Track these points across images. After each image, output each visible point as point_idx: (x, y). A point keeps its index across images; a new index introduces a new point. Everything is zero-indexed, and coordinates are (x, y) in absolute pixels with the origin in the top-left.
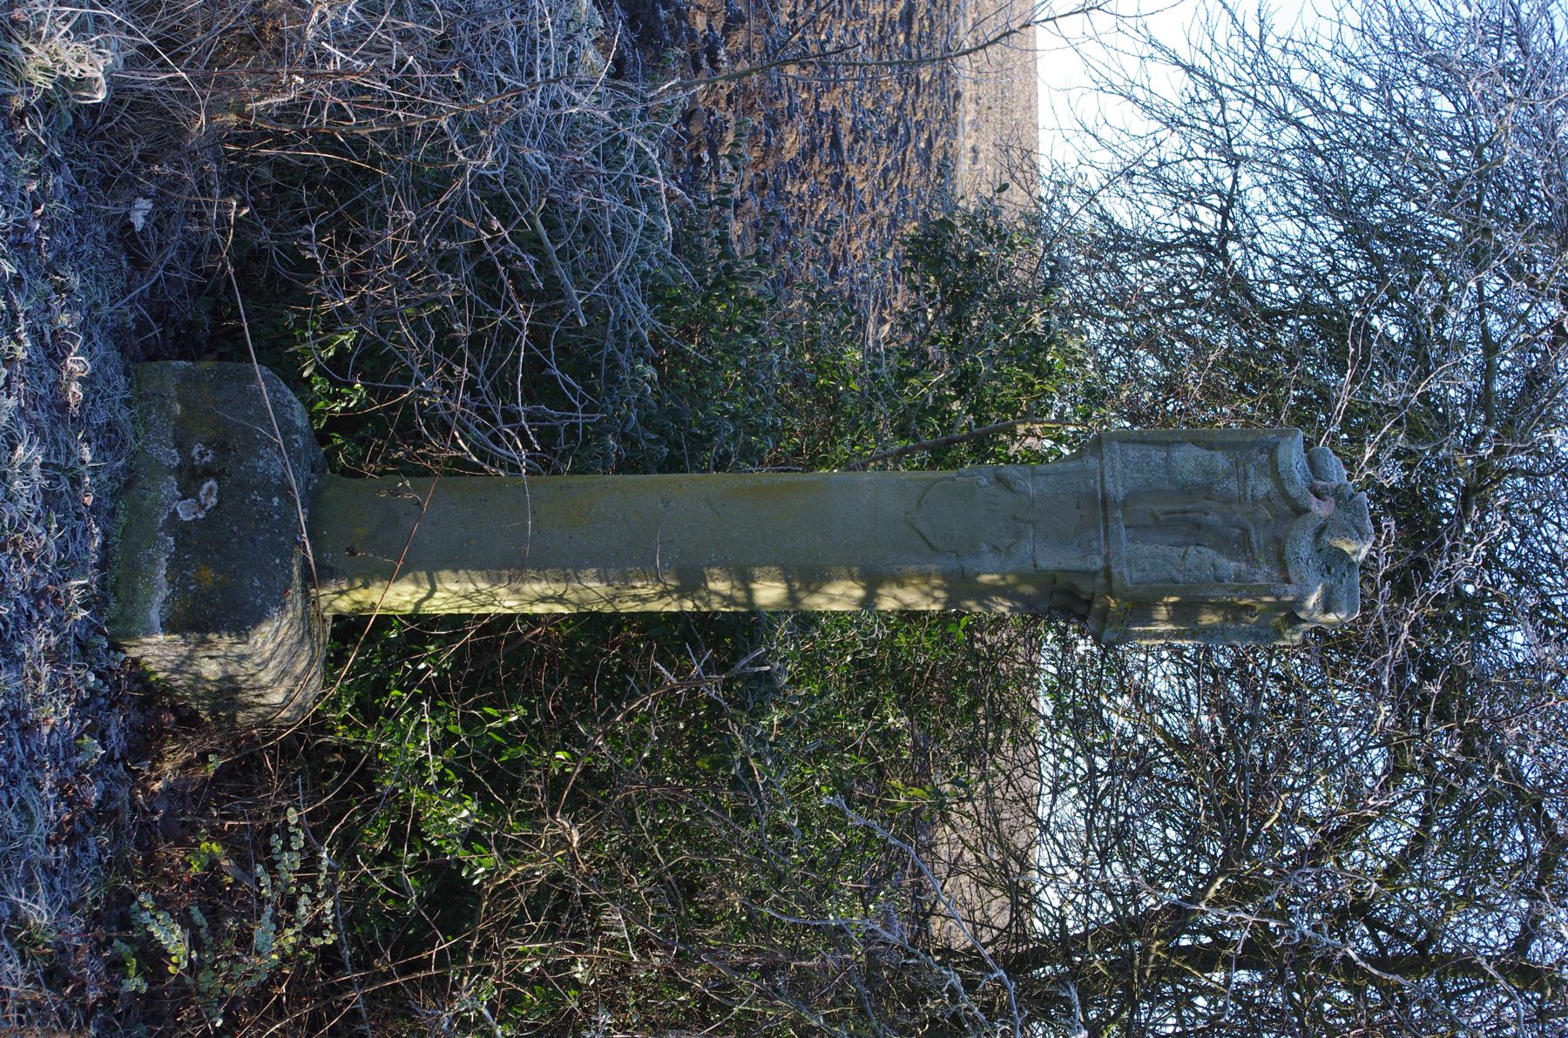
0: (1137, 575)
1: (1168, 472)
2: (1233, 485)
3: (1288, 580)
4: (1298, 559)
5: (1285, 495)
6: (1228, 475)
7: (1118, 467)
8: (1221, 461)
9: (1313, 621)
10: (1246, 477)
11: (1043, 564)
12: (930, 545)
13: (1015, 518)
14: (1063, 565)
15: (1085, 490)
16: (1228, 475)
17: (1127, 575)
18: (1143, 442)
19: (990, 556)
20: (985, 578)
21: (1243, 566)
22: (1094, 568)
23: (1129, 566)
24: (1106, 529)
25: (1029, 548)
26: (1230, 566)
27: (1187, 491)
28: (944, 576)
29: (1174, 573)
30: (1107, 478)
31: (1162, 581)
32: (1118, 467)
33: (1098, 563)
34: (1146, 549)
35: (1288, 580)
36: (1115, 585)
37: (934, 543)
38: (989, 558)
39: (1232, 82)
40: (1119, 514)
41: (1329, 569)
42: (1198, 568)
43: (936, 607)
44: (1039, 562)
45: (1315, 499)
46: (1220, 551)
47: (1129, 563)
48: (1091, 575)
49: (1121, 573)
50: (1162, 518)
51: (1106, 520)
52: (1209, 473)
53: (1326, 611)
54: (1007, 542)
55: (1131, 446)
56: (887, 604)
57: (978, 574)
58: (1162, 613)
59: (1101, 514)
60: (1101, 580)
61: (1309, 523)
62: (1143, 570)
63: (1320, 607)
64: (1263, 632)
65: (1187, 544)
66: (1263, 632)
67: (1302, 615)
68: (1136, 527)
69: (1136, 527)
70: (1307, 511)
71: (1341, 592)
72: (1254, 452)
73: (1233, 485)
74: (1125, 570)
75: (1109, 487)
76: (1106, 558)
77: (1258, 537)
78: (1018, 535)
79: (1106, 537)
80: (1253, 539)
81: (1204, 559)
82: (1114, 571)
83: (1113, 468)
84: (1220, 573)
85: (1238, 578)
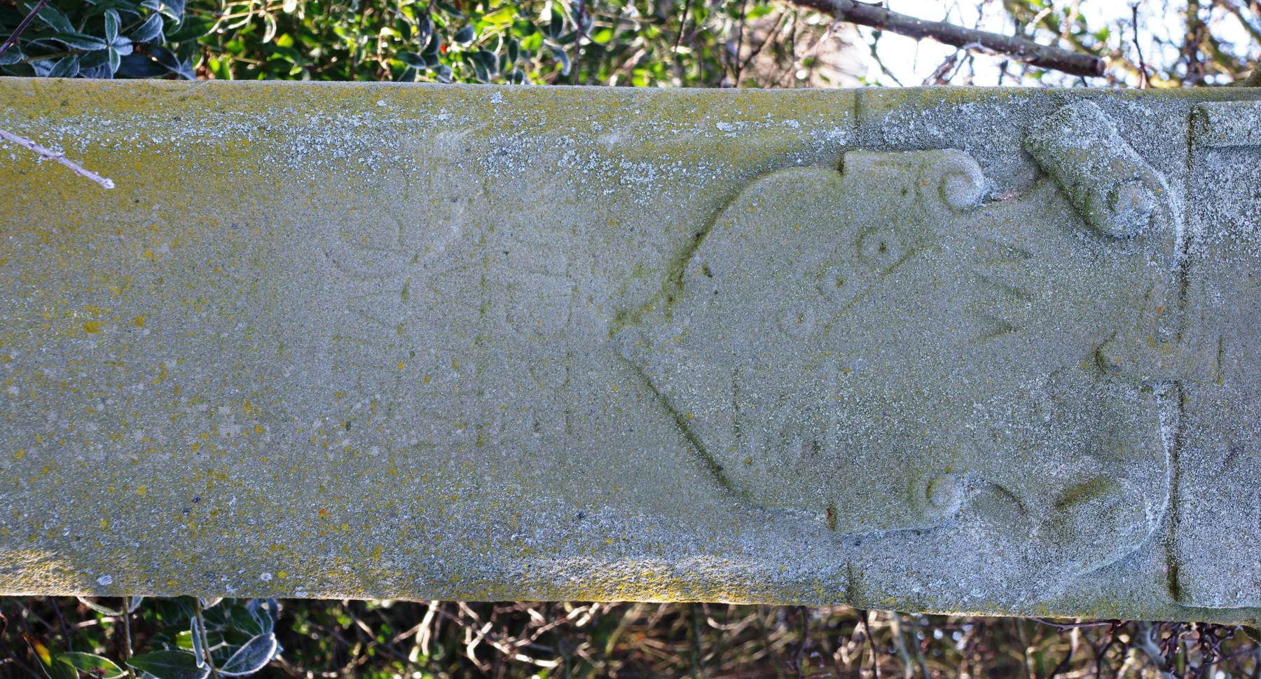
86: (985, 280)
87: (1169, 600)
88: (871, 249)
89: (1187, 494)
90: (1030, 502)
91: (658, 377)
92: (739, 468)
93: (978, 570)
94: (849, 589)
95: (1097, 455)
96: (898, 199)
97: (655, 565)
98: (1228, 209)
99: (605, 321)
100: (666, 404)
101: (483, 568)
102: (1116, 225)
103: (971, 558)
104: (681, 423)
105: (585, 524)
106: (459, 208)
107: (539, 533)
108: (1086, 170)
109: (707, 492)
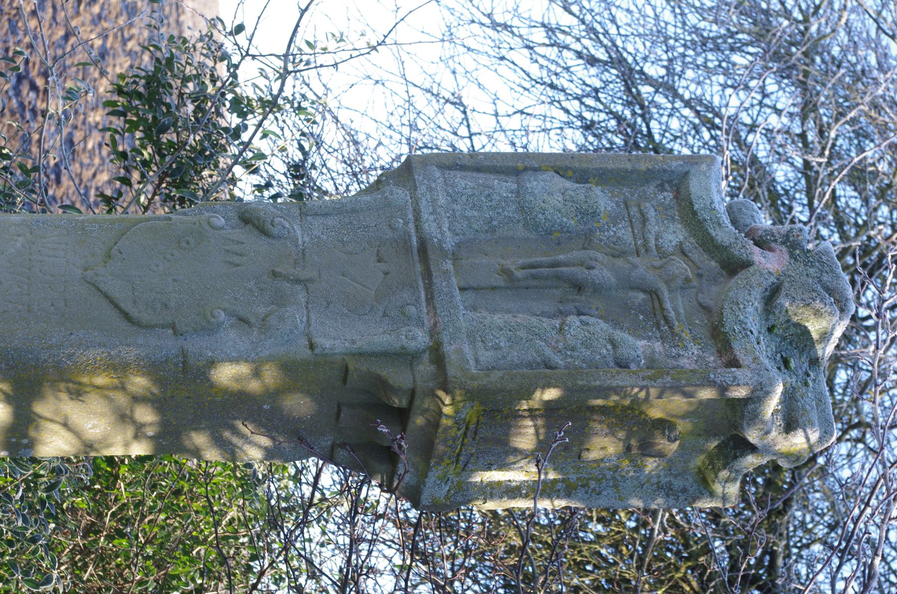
0: (486, 356)
1: (522, 209)
2: (624, 233)
3: (734, 363)
4: (746, 332)
5: (710, 246)
6: (614, 220)
7: (442, 201)
8: (603, 199)
9: (767, 450)
10: (644, 220)
11: (325, 343)
12: (127, 316)
13: (275, 274)
14: (362, 344)
15: (390, 234)
16: (614, 220)
17: (467, 356)
18: (478, 169)
19: (232, 334)
20: (227, 374)
21: (658, 346)
22: (412, 345)
23: (473, 342)
24: (429, 287)
25: (299, 318)
26: (639, 346)
27: (551, 235)
28: (152, 369)
29: (548, 352)
30: (425, 216)
31: (529, 365)
32: (442, 201)
33: (420, 339)
34: (498, 319)
35: (734, 363)
36: (451, 371)
37: (134, 312)
38: (231, 337)
39: (468, 61)
40: (449, 266)
41: (786, 363)
42: (587, 344)
43: (139, 449)
44: (318, 340)
45: (757, 249)
46: (616, 324)
47: (471, 337)
48: (407, 357)
49: (459, 351)
50: (519, 274)
51: (428, 275)
52: (588, 214)
53: (790, 426)
54: (262, 310)
55: (459, 174)
56: (54, 444)
57: (212, 363)
58: (526, 437)
59: (419, 268)
60: (425, 367)
61: (754, 280)
62: (497, 348)
63: (779, 422)
64: (678, 483)
65: (563, 314)
66: (678, 483)
67: (753, 436)
68: (475, 289)
69: (475, 289)
70: (746, 264)
71: (808, 400)
72: (651, 189)
73: (624, 233)
74: (467, 349)
75: (430, 227)
76: (433, 332)
77: (675, 305)
78: (280, 300)
79: (430, 300)
80: (668, 305)
81: (590, 333)
82: (449, 349)
83: (434, 201)
84: (623, 352)
85: (652, 363)
86: (228, 251)
87: (309, 352)
88: (184, 244)
89: (313, 317)
90: (253, 320)
91: (102, 286)
92: (136, 314)
93: (234, 347)
94: (183, 363)
95: (276, 304)
96: (193, 226)
97: (103, 353)
98: (316, 232)
99: (79, 272)
100: (107, 296)
101: (30, 356)
102: (275, 231)
103: (231, 343)
104: (112, 302)
105: (73, 337)
106: (21, 239)
107: (54, 340)
108: (262, 214)
109: (124, 325)
